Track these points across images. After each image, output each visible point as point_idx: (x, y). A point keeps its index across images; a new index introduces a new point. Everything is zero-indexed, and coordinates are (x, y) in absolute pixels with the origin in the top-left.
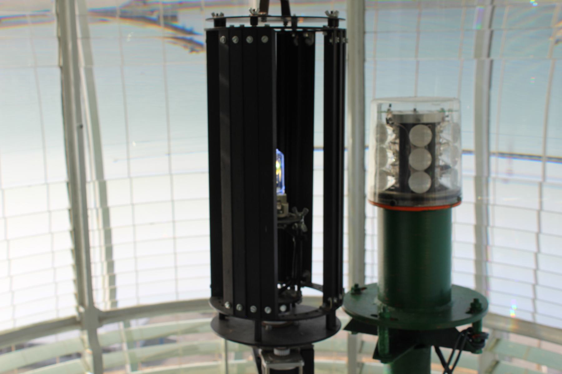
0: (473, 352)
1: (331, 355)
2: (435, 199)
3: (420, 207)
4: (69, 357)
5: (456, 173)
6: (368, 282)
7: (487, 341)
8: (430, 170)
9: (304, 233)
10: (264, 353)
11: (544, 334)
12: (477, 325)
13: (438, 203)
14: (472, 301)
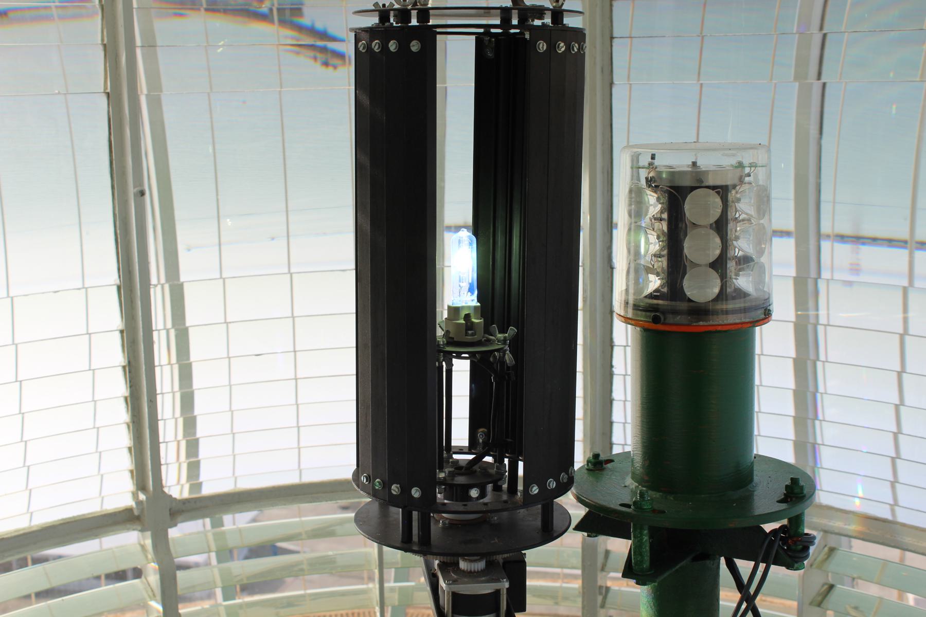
0: (789, 567)
1: (555, 570)
2: (727, 312)
3: (702, 324)
4: (119, 576)
5: (762, 268)
6: (617, 450)
7: (812, 549)
8: (719, 265)
9: (508, 368)
10: (443, 566)
11: (908, 540)
12: (797, 521)
13: (732, 319)
14: (788, 482)
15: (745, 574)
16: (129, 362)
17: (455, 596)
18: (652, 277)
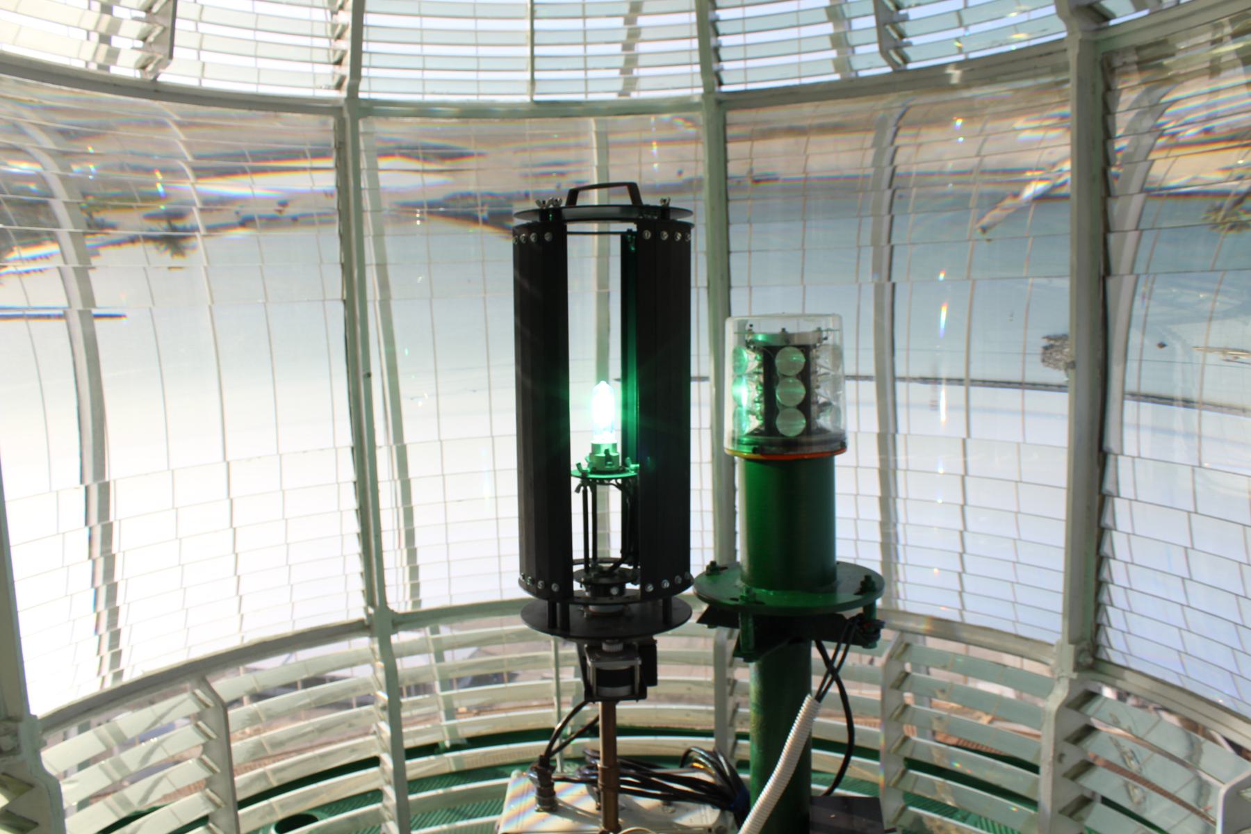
2: (810, 444)
10: (590, 650)
12: (870, 608)
13: (816, 449)
14: (863, 579)
15: (830, 653)
17: (599, 672)
18: (752, 418)
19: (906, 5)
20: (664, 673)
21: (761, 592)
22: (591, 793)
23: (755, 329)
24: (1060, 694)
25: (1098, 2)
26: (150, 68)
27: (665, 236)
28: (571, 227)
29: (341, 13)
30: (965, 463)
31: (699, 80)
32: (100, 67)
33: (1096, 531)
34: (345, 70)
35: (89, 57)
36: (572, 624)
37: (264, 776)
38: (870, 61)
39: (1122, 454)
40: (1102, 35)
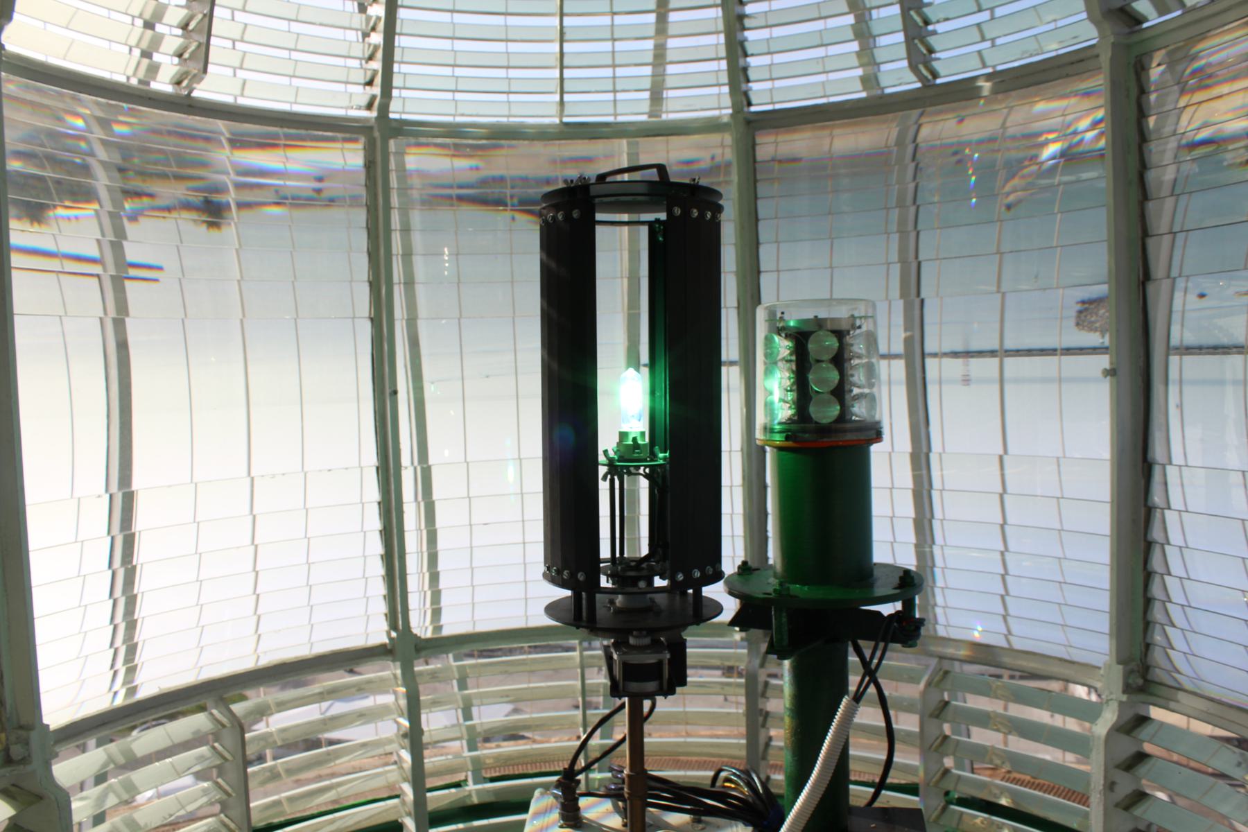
2: (845, 431)
12: (909, 605)
13: (850, 437)
16: (385, 528)
17: (626, 666)
19: (934, 20)
20: (692, 677)
21: (796, 589)
22: (617, 809)
23: (786, 317)
24: (1109, 717)
25: (1129, 4)
26: (185, 83)
27: (695, 213)
28: (599, 216)
29: (373, 34)
30: (1003, 476)
31: (727, 101)
32: (140, 82)
33: (1142, 544)
34: (376, 90)
35: (130, 72)
36: (598, 617)
37: (277, 803)
38: (898, 77)
39: (1170, 463)
40: (1136, 38)
